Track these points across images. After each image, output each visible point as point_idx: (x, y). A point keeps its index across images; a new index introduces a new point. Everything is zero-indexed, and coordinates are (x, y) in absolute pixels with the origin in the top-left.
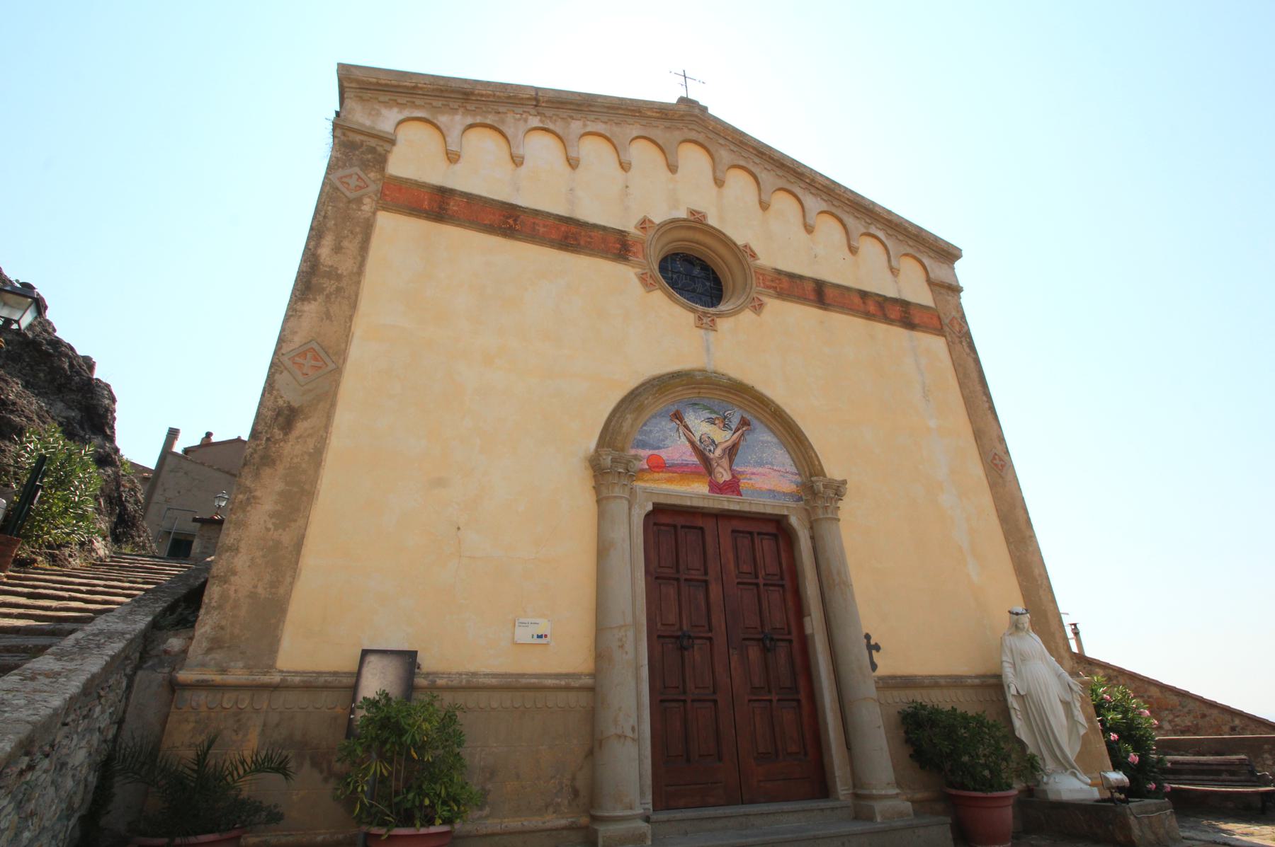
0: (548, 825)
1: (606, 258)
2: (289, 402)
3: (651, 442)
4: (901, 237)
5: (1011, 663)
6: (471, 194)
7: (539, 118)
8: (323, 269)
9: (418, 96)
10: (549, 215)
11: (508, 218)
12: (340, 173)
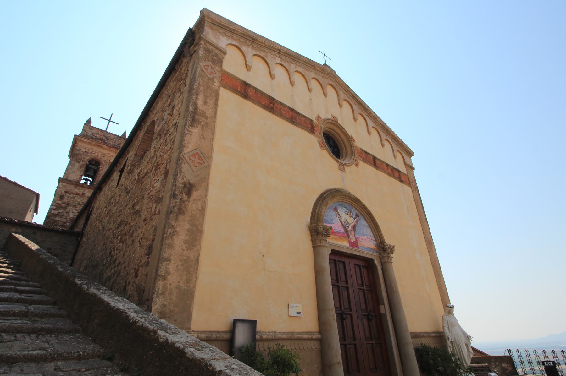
2: (189, 180)
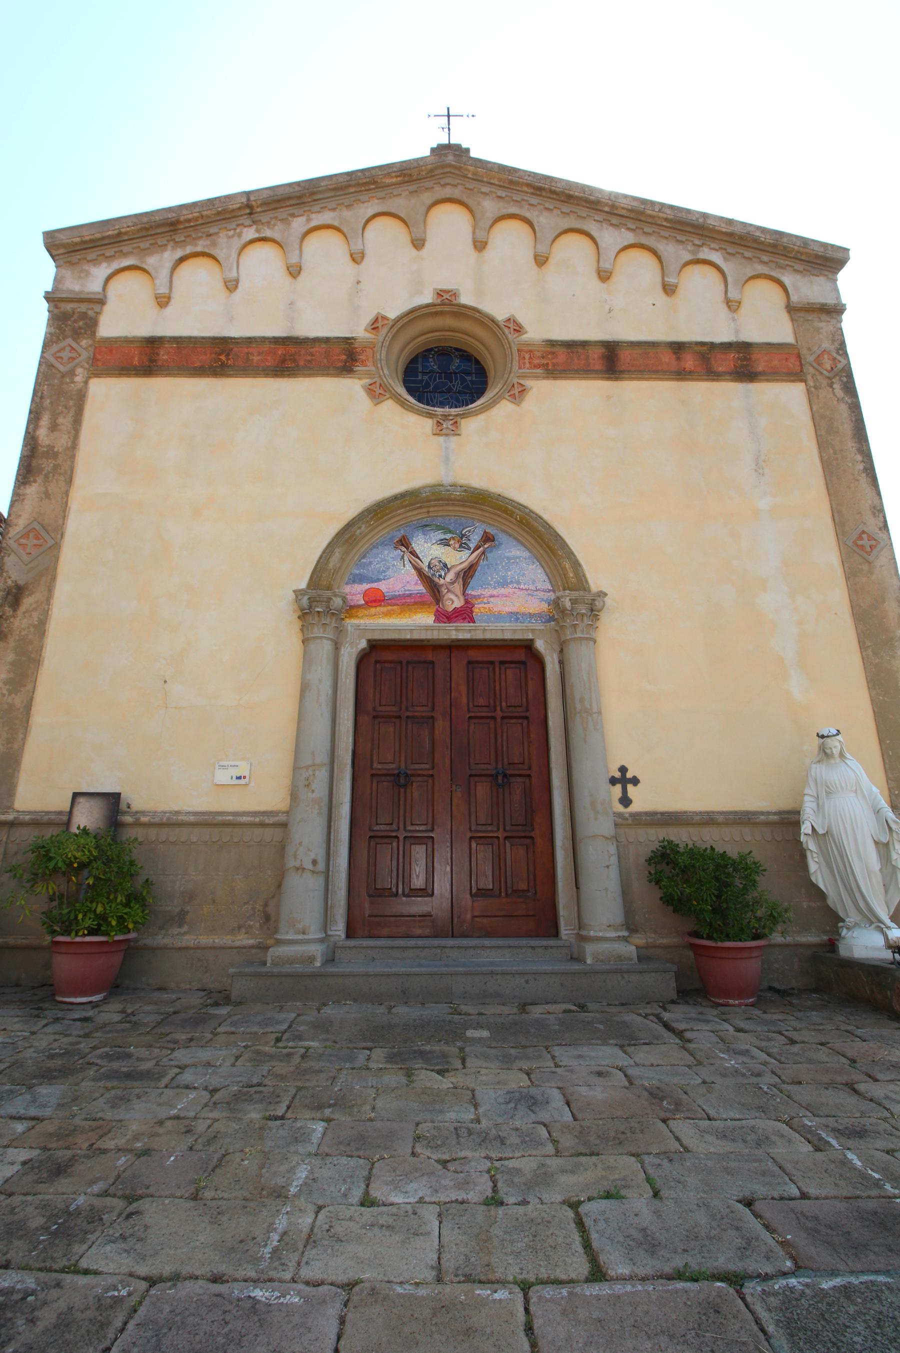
0: (238, 943)
1: (327, 375)
2: (16, 582)
3: (370, 575)
4: (748, 254)
5: (814, 796)
6: (180, 338)
7: (255, 227)
8: (41, 449)
9: (124, 243)
10: (263, 339)
11: (220, 354)
12: (55, 348)
